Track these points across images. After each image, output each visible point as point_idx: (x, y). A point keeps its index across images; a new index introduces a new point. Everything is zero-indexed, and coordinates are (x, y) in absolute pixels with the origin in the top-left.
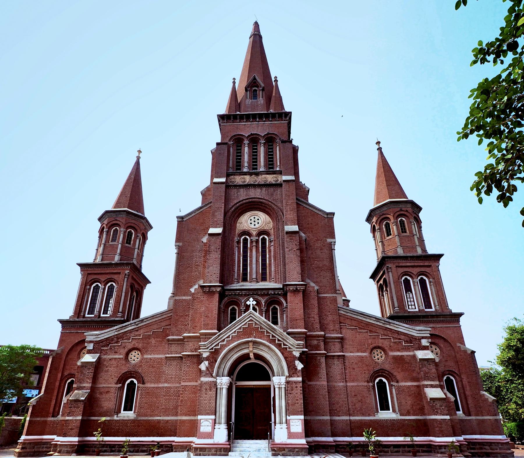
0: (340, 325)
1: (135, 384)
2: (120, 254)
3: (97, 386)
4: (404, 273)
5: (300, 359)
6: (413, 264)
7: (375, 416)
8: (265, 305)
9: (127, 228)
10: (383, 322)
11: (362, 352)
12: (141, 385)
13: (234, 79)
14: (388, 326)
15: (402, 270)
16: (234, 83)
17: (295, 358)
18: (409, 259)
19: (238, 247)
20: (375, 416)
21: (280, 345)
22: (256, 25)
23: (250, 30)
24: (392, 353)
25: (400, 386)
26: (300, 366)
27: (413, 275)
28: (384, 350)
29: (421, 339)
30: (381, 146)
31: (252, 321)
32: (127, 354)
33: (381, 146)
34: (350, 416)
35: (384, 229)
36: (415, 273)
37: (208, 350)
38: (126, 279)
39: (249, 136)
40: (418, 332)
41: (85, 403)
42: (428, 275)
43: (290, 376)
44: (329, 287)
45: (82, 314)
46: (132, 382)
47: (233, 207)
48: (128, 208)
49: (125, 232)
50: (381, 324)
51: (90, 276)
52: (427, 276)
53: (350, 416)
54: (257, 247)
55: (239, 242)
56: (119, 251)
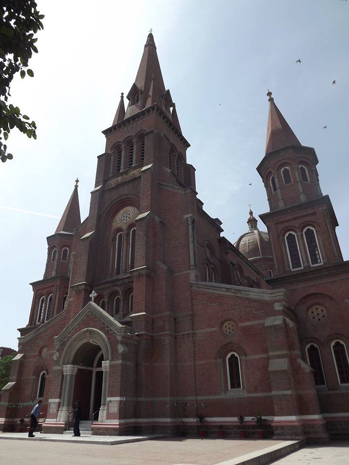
0: (192, 302)
1: (316, 348)
2: (56, 270)
3: (23, 378)
4: (286, 229)
5: (122, 343)
6: (294, 216)
7: (221, 395)
8: (122, 294)
9: (62, 247)
10: (233, 291)
11: (211, 327)
12: (244, 358)
13: (122, 94)
14: (239, 295)
15: (281, 226)
16: (122, 97)
17: (117, 342)
18: (289, 211)
19: (113, 244)
20: (221, 395)
21: (108, 331)
22: (151, 37)
23: (144, 41)
24: (241, 324)
25: (249, 360)
26: (121, 349)
27: (295, 229)
28: (235, 322)
29: (273, 303)
30: (272, 96)
31: (91, 312)
32: (41, 351)
33: (272, 96)
34: (196, 396)
35: (271, 185)
36: (297, 225)
37: (59, 343)
38: (58, 289)
39: (124, 141)
40: (270, 296)
41: (10, 393)
42: (314, 224)
43: (112, 360)
44: (184, 264)
45: (33, 323)
46: (233, 356)
47: (107, 207)
48: (63, 231)
49: (60, 251)
50: (232, 294)
51: (38, 292)
52: (314, 226)
53: (196, 396)
54: (128, 240)
55: (114, 240)
56: (55, 268)
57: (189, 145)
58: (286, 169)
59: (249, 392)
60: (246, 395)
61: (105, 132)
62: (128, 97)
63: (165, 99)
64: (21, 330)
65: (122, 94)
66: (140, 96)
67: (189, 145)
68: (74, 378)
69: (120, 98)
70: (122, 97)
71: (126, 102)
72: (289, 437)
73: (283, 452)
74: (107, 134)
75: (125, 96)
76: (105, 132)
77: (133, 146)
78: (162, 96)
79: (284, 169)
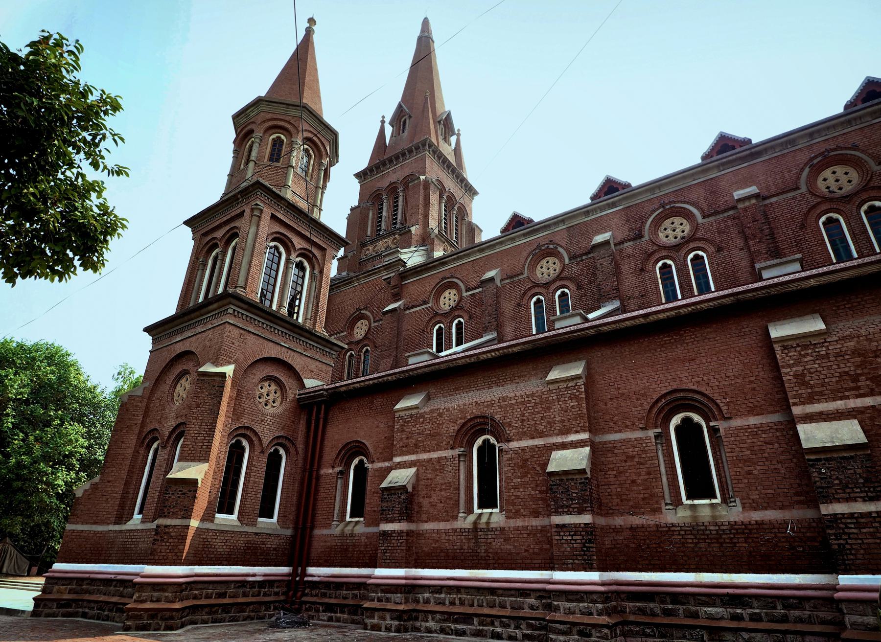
16: (383, 122)
57: (475, 193)
58: (488, 440)
59: (750, 505)
60: (734, 514)
61: (358, 175)
62: (391, 124)
63: (444, 125)
64: (150, 351)
65: (383, 117)
66: (407, 122)
67: (475, 193)
68: (320, 518)
69: (380, 124)
70: (383, 122)
71: (389, 130)
72: (225, 563)
73: (393, 589)
74: (361, 177)
75: (388, 120)
76: (358, 175)
77: (397, 198)
78: (439, 122)
79: (484, 441)
